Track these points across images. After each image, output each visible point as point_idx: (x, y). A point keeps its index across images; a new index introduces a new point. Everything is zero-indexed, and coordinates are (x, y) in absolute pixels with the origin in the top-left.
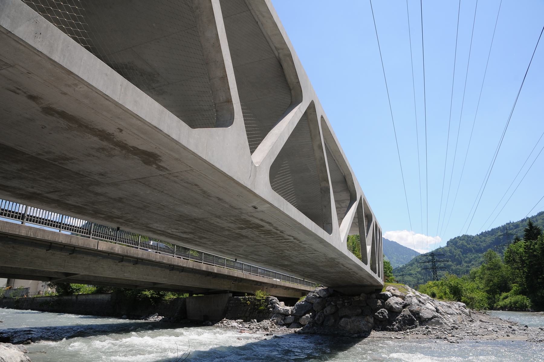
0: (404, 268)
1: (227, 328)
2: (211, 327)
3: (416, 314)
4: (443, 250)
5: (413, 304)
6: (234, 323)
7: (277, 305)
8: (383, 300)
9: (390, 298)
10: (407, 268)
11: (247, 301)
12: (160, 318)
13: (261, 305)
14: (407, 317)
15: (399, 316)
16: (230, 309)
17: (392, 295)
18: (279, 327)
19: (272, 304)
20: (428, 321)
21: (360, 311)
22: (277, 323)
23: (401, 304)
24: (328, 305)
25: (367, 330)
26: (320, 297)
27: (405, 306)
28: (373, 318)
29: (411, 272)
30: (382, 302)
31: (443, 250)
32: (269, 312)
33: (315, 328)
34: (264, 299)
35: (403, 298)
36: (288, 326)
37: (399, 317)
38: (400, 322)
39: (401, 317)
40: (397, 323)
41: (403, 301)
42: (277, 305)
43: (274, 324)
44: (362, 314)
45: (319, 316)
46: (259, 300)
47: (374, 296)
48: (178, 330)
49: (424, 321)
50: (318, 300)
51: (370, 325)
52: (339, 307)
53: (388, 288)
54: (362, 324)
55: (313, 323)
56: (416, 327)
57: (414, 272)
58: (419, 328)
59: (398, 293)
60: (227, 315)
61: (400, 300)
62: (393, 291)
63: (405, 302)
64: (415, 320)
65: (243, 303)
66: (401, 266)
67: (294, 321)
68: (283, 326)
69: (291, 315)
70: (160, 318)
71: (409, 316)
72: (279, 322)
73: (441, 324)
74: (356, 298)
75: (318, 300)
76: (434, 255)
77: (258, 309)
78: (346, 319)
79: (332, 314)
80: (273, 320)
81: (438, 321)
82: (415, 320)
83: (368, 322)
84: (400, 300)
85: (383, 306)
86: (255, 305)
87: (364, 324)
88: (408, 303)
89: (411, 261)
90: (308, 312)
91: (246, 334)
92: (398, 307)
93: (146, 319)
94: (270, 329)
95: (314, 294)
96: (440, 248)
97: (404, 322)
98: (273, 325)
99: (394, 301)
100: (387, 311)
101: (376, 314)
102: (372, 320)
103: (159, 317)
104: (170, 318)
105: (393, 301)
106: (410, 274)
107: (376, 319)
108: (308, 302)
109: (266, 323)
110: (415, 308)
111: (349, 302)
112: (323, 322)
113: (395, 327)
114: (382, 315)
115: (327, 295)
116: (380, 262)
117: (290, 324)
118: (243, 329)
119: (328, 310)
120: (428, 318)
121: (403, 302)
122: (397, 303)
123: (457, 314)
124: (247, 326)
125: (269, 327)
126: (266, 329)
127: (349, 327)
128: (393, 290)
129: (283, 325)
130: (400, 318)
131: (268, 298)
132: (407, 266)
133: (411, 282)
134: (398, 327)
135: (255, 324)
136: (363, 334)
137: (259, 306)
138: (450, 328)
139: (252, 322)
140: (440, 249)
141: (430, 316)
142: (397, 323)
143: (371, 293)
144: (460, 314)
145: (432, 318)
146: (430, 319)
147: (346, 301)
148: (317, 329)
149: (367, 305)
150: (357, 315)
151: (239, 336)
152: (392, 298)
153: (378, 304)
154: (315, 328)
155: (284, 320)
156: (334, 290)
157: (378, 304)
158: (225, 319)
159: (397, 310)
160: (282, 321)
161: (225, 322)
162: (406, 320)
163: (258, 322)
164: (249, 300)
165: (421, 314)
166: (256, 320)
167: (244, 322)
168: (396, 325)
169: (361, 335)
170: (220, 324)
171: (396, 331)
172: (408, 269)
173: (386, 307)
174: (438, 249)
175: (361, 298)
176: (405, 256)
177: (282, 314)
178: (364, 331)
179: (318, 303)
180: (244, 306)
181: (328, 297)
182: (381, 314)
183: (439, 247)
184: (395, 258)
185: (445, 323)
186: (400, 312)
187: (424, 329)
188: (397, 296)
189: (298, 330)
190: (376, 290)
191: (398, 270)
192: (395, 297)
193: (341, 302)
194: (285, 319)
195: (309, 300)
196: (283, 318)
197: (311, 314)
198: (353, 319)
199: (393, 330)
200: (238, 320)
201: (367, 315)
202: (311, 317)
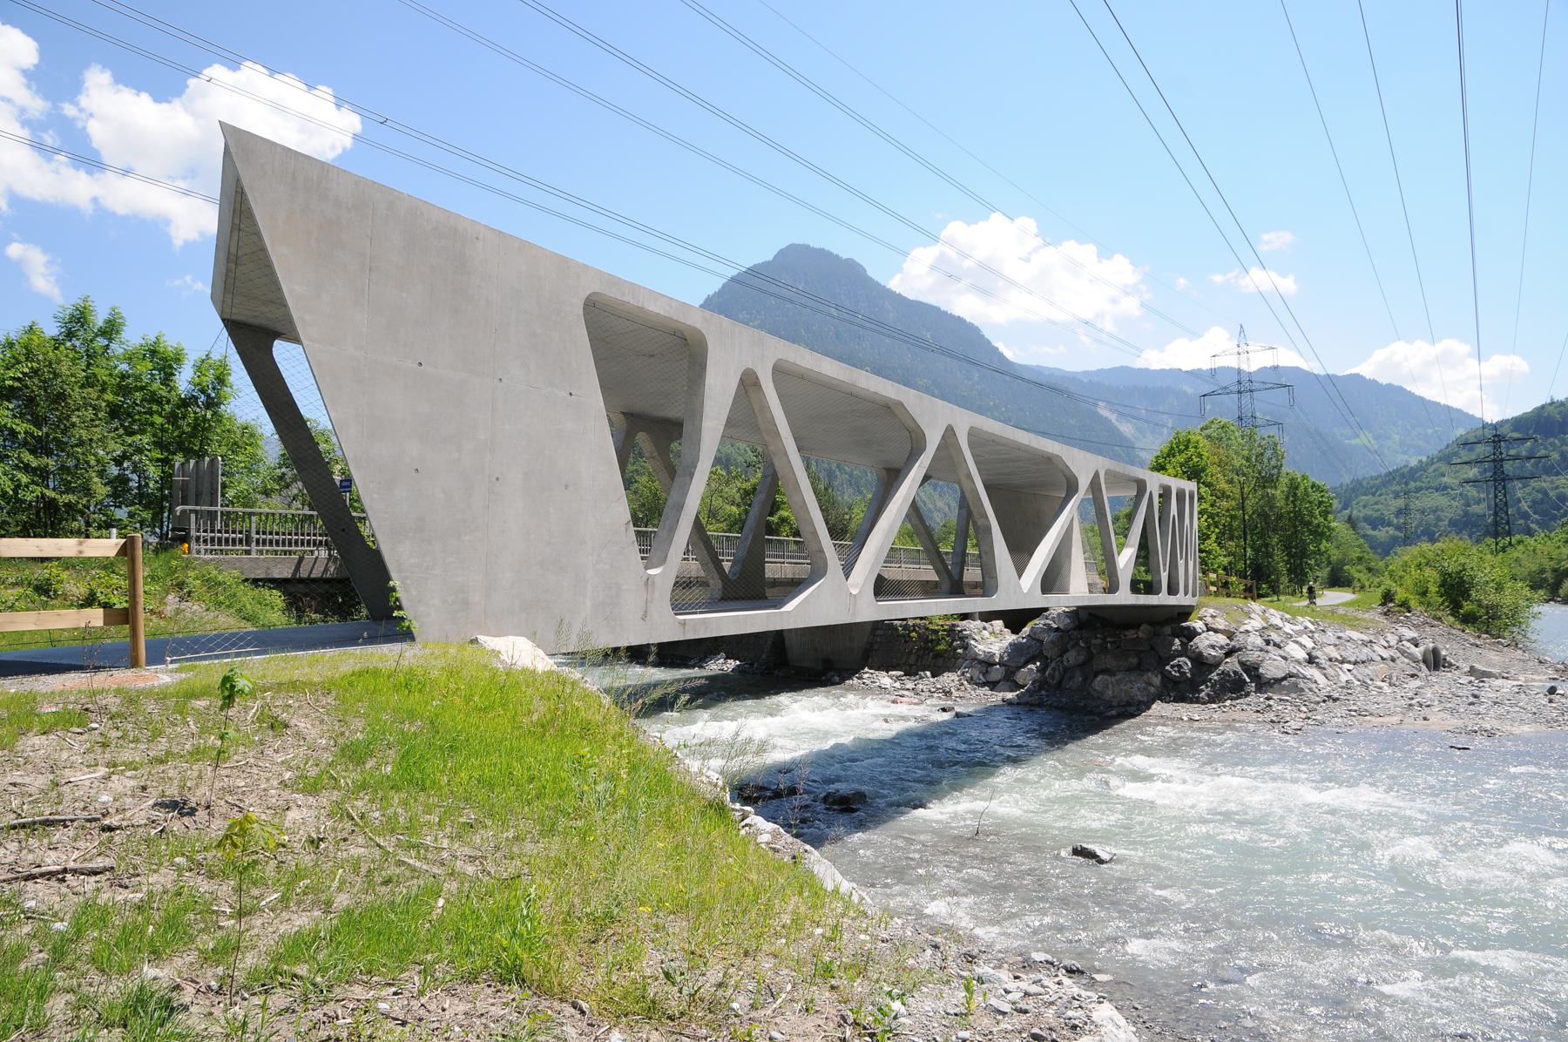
0: (1422, 468)
1: (867, 691)
2: (835, 690)
3: (1252, 669)
4: (1562, 408)
5: (1250, 648)
6: (885, 679)
7: (973, 642)
8: (1185, 640)
9: (1200, 634)
10: (1431, 470)
11: (910, 632)
12: (732, 664)
13: (938, 642)
14: (1230, 676)
15: (1215, 674)
16: (876, 647)
17: (1205, 629)
18: (975, 689)
19: (962, 639)
20: (1274, 684)
21: (1134, 661)
22: (970, 681)
23: (1222, 648)
24: (1073, 647)
25: (1145, 699)
26: (1057, 629)
27: (1229, 654)
28: (1160, 677)
29: (1445, 479)
30: (1183, 644)
31: (1562, 408)
32: (956, 657)
33: (1043, 692)
34: (945, 630)
35: (1230, 636)
36: (993, 686)
37: (1214, 676)
38: (1213, 686)
39: (1218, 674)
40: (1207, 687)
41: (1228, 641)
42: (973, 642)
43: (965, 683)
44: (1139, 669)
45: (1054, 669)
46: (935, 632)
47: (1167, 630)
48: (770, 701)
49: (1263, 684)
50: (1053, 635)
51: (1152, 689)
52: (1095, 651)
53: (1202, 612)
54: (1135, 688)
55: (1041, 684)
56: (1247, 695)
57: (1454, 481)
58: (1252, 698)
59: (1221, 624)
60: (870, 660)
61: (1221, 639)
62: (1209, 620)
63: (1233, 643)
64: (1248, 680)
65: (903, 636)
66: (1413, 463)
67: (1004, 678)
68: (983, 687)
69: (999, 664)
70: (732, 664)
71: (1235, 672)
72: (975, 678)
73: (1302, 690)
74: (1131, 634)
75: (1053, 635)
76: (1500, 441)
77: (932, 650)
78: (1106, 677)
79: (1079, 665)
80: (963, 674)
81: (1296, 685)
82: (1248, 680)
83: (1150, 684)
84: (1221, 639)
85: (1184, 652)
86: (927, 641)
87: (1139, 689)
88: (1237, 646)
89: (1448, 446)
90: (1032, 660)
91: (902, 709)
92: (1213, 653)
93: (701, 667)
94: (955, 694)
95: (1048, 621)
96: (1552, 403)
97: (1223, 686)
98: (962, 684)
99: (1207, 643)
100: (1189, 664)
101: (1168, 668)
102: (1157, 680)
103: (729, 661)
104: (752, 664)
105: (1207, 643)
106: (1443, 489)
107: (1166, 677)
108: (1034, 639)
109: (949, 679)
110: (1253, 657)
111: (1114, 642)
112: (1060, 682)
113: (1202, 695)
114: (1179, 671)
115: (1072, 626)
116: (1181, 563)
117: (998, 682)
118: (901, 692)
119: (1072, 657)
120: (1274, 679)
121: (1228, 645)
122: (1213, 647)
123: (1383, 659)
124: (910, 685)
125: (952, 690)
126: (947, 693)
127: (1110, 692)
128: (1212, 616)
129: (983, 685)
130: (1216, 678)
131: (954, 625)
132: (1433, 464)
133: (1443, 511)
134: (1208, 695)
135: (927, 680)
136: (1132, 710)
137: (935, 643)
138: (1317, 699)
139: (921, 678)
140: (1552, 408)
141: (1280, 675)
142: (1207, 687)
143: (1163, 623)
144: (1393, 660)
145: (1284, 678)
146: (1279, 681)
147: (1109, 639)
148: (1047, 696)
149: (1152, 648)
150: (1129, 670)
151: (887, 711)
152: (1204, 635)
153: (1173, 648)
154: (1043, 692)
155: (985, 674)
156: (1090, 614)
157: (1173, 648)
158: (866, 669)
159: (1211, 661)
160: (981, 677)
161: (866, 676)
162: (1228, 681)
163: (933, 676)
164: (914, 630)
165: (1261, 670)
166: (928, 673)
167: (905, 675)
168: (1205, 691)
169: (1131, 709)
170: (855, 681)
171: (1204, 703)
172: (1434, 471)
173: (1189, 654)
174: (1543, 407)
175: (1141, 634)
176: (1430, 431)
177: (981, 662)
178: (1140, 702)
179: (1052, 642)
180: (906, 642)
181: (1074, 629)
182: (1176, 669)
183: (1549, 401)
184: (1398, 436)
185: (1310, 690)
186: (1219, 664)
187: (1262, 700)
188: (1216, 631)
189: (1010, 695)
190: (1179, 614)
191: (1403, 476)
192: (1211, 633)
193: (1099, 641)
194: (987, 672)
195: (1035, 634)
196: (984, 670)
197: (1038, 664)
198: (1118, 677)
199: (1198, 701)
200: (894, 673)
201: (1149, 670)
202: (1038, 671)
